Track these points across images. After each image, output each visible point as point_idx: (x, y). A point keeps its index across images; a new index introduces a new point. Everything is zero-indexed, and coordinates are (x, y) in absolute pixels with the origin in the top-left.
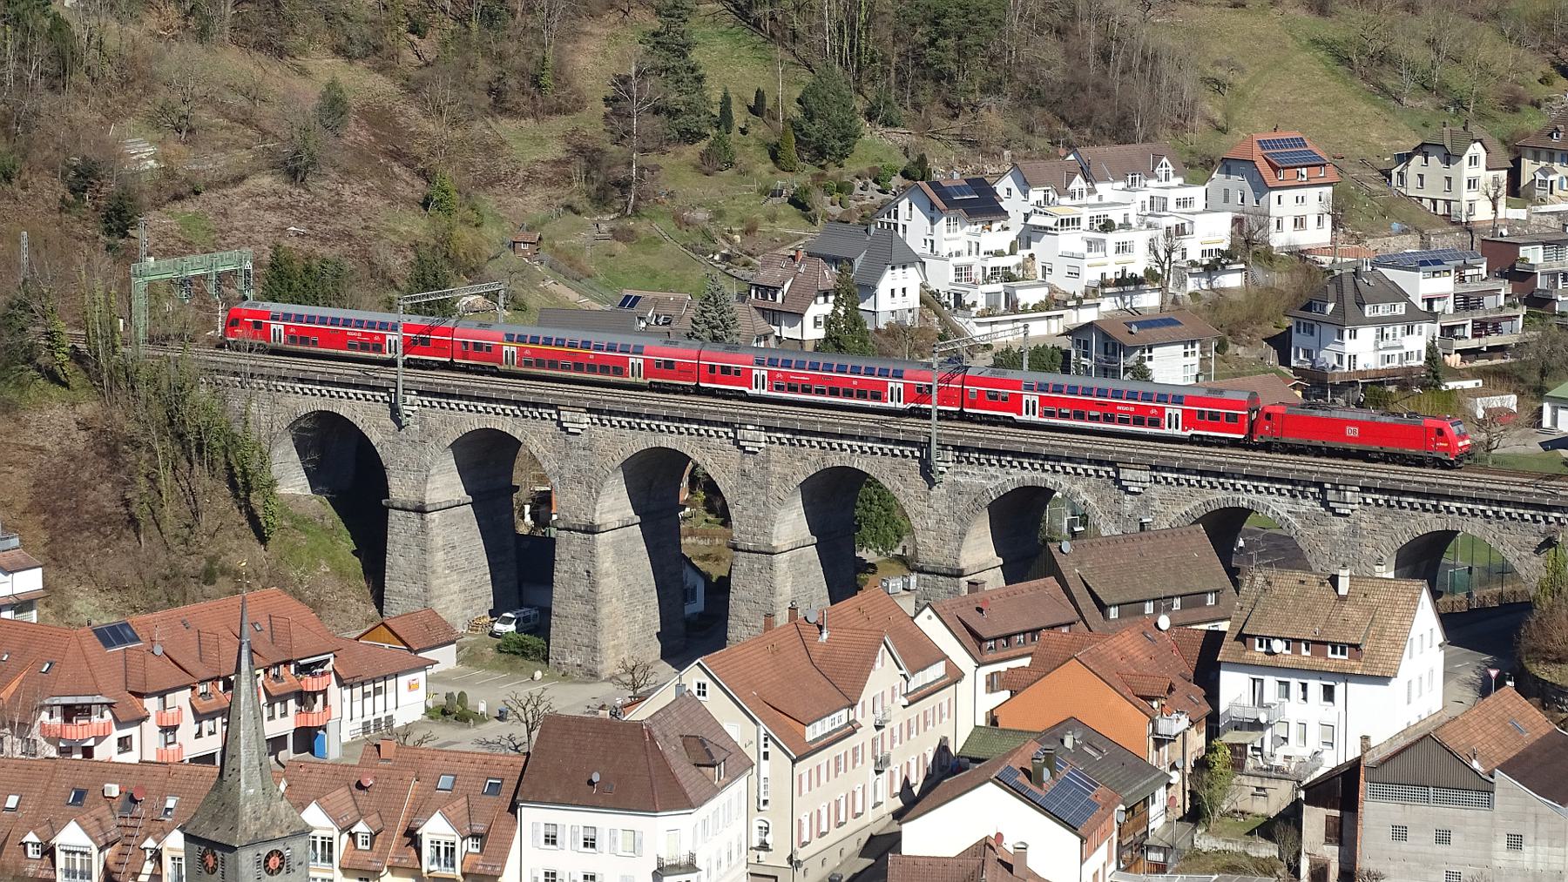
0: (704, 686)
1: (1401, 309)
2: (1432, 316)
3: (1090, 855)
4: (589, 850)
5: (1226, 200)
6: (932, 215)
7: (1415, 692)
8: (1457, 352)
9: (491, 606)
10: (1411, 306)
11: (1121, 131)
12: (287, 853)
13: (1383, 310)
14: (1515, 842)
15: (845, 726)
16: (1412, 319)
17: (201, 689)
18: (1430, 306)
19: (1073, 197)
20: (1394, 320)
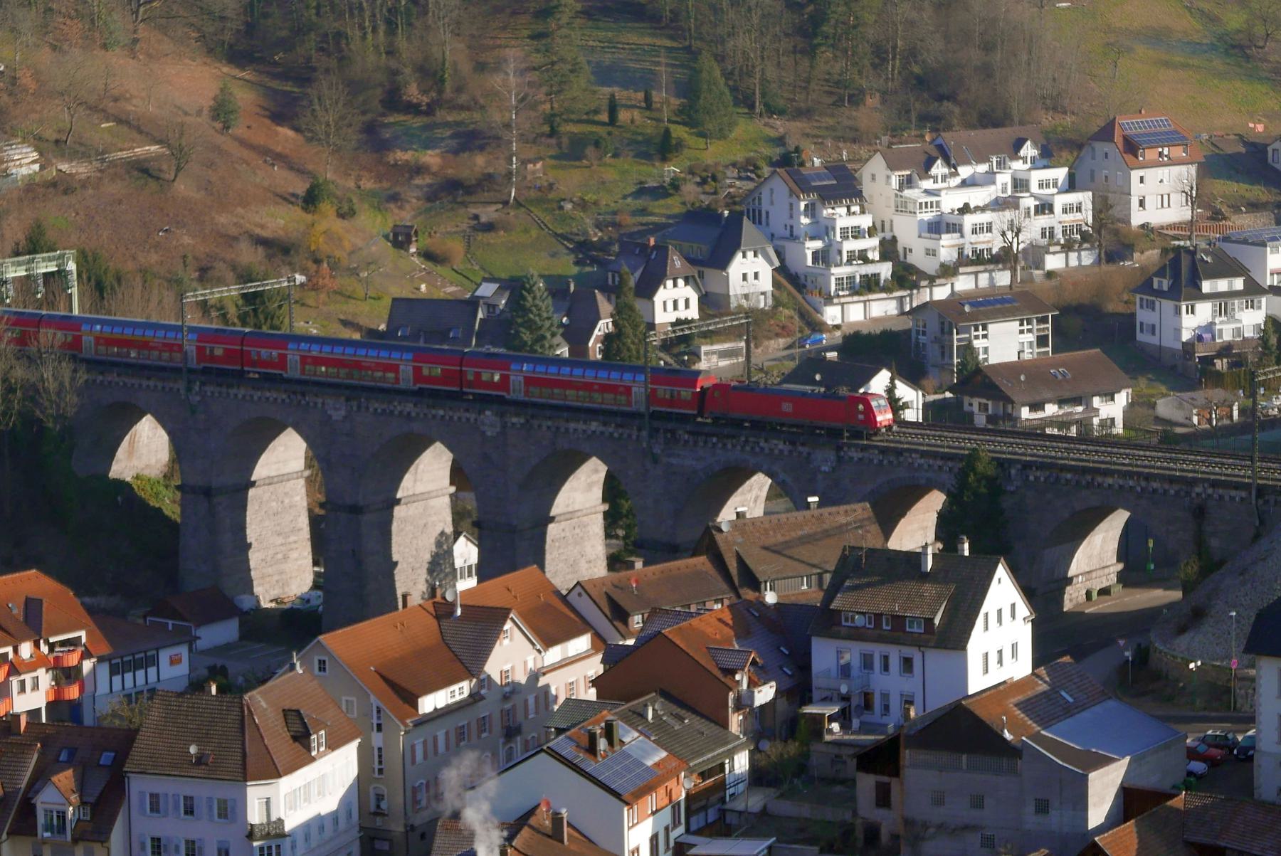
0: (324, 661)
1: (1239, 284)
3: (642, 821)
4: (155, 815)
9: (1068, 588)
11: (991, 118)
13: (1222, 285)
14: (1043, 807)
19: (936, 181)
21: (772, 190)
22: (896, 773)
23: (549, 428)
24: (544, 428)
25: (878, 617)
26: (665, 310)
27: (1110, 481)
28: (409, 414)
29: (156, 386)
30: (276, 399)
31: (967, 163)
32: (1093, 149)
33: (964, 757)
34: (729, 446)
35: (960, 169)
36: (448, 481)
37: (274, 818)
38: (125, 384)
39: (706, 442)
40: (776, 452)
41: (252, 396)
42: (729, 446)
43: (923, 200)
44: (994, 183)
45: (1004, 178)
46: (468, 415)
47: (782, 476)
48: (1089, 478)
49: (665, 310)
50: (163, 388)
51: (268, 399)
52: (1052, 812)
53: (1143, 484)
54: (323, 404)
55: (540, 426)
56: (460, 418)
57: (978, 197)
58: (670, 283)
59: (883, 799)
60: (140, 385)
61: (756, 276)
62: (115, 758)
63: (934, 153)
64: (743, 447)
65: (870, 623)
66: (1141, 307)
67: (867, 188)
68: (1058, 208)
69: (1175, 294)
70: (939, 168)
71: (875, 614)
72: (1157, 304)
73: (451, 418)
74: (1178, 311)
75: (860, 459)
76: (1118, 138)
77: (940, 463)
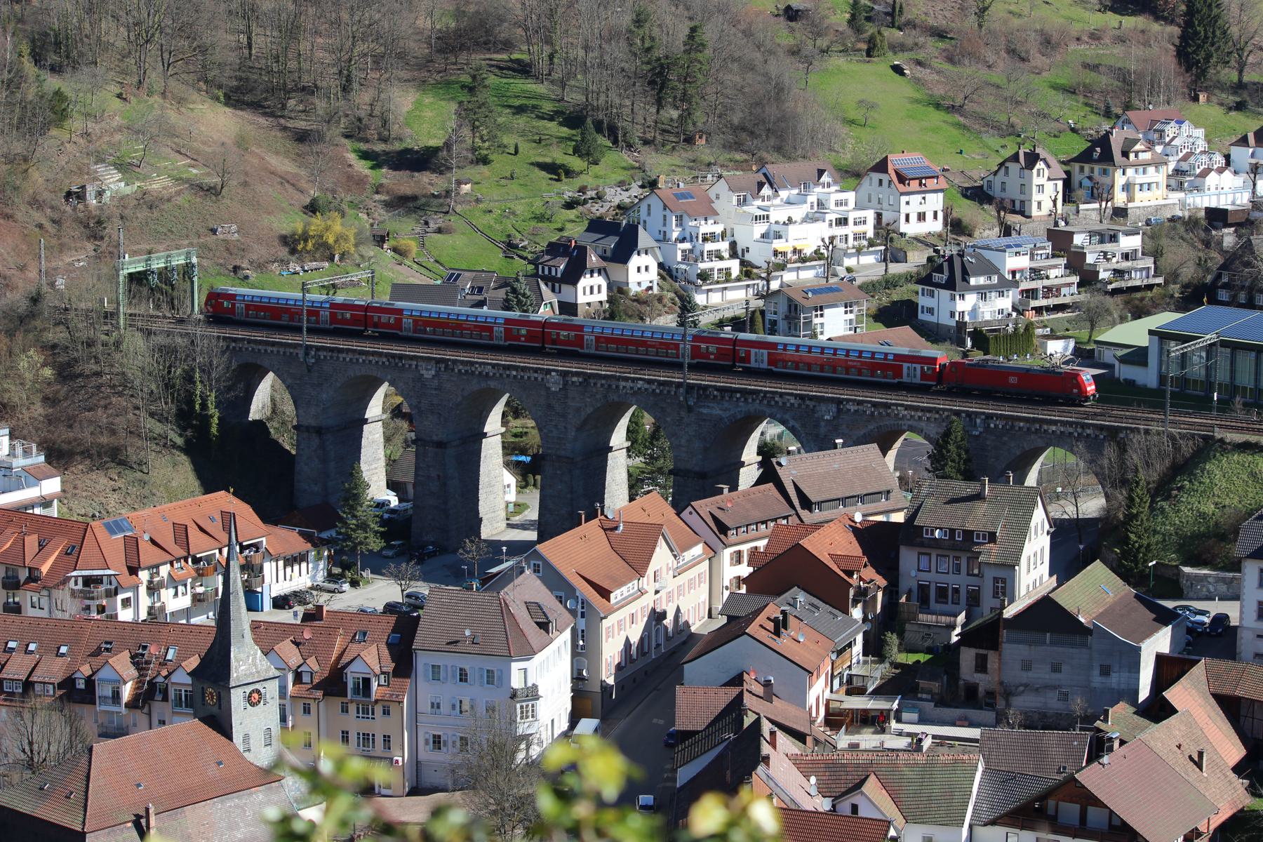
2: (1015, 284)
5: (870, 201)
6: (665, 213)
7: (1032, 567)
8: (1033, 309)
10: (1001, 277)
12: (263, 691)
13: (982, 280)
14: (1106, 671)
15: (636, 593)
16: (1003, 286)
17: (176, 565)
18: (1014, 276)
19: (763, 200)
20: (991, 288)
21: (649, 206)
22: (995, 646)
23: (602, 385)
24: (599, 385)
25: (952, 531)
26: (584, 294)
27: (1054, 428)
28: (487, 373)
29: (278, 352)
30: (377, 362)
31: (785, 187)
32: (871, 179)
33: (1048, 635)
34: (750, 400)
35: (780, 192)
36: (499, 424)
37: (529, 684)
38: (253, 349)
39: (731, 397)
40: (788, 405)
41: (357, 360)
42: (750, 400)
43: (758, 214)
44: (805, 202)
45: (812, 198)
46: (536, 375)
47: (792, 423)
48: (1037, 426)
49: (584, 294)
50: (284, 353)
51: (370, 361)
52: (1113, 675)
53: (1079, 430)
54: (417, 366)
55: (595, 384)
56: (529, 378)
57: (798, 212)
58: (588, 276)
59: (981, 666)
60: (266, 350)
61: (647, 268)
62: (401, 637)
63: (764, 180)
64: (761, 401)
65: (945, 535)
66: (923, 295)
67: (717, 206)
68: (851, 221)
69: (950, 285)
70: (766, 191)
71: (950, 529)
72: (936, 292)
73: (522, 377)
74: (953, 298)
75: (856, 411)
76: (890, 170)
77: (920, 414)
